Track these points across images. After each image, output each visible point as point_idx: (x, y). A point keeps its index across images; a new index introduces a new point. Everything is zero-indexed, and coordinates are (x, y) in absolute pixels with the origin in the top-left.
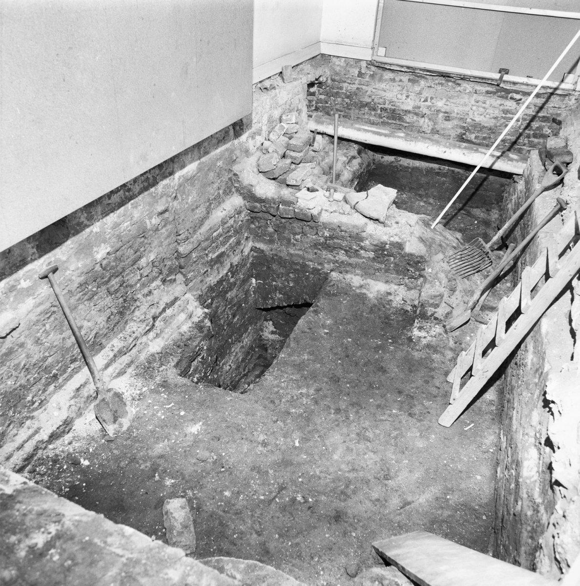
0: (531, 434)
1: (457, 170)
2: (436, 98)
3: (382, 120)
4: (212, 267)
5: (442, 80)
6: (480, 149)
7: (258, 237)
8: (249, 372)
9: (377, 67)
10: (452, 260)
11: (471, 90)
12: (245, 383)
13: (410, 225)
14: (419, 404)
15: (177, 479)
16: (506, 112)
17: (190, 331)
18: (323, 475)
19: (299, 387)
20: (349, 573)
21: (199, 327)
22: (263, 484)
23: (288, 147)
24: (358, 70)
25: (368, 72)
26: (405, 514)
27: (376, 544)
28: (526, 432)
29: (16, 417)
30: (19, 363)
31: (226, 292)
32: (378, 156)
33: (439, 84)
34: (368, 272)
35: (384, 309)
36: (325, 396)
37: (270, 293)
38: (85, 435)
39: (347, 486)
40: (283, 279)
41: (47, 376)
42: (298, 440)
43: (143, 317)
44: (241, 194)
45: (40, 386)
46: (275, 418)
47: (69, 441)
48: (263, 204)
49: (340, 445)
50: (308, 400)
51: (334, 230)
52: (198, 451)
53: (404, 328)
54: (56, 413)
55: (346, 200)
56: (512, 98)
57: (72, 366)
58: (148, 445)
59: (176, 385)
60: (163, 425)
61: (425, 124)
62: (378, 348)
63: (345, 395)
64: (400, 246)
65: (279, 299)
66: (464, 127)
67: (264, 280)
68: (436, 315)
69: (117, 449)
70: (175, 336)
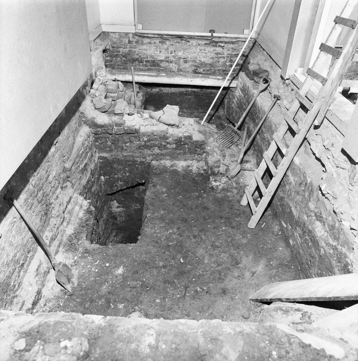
0: (312, 215)
1: (194, 90)
2: (177, 50)
3: (147, 68)
4: (83, 173)
5: (179, 40)
6: (209, 77)
7: (101, 149)
8: (109, 235)
9: (139, 36)
10: (218, 140)
11: (196, 44)
12: (109, 242)
13: (191, 125)
14: (234, 221)
15: (125, 303)
16: (217, 54)
17: (84, 216)
18: (204, 273)
19: (167, 230)
20: (245, 317)
21: (88, 212)
22: (175, 289)
23: (107, 91)
24: (128, 39)
25: (134, 40)
26: (256, 278)
27: (251, 297)
28: (309, 215)
29: (8, 298)
30: (4, 262)
31: (91, 188)
32: (149, 90)
33: (177, 42)
34: (173, 156)
35: (190, 175)
36: (183, 231)
37: (114, 183)
38: (52, 297)
39: (220, 275)
40: (122, 172)
41: (18, 266)
42: (182, 259)
43: (57, 214)
44: (87, 125)
45: (16, 274)
46: (163, 251)
47: (44, 304)
48: (103, 129)
49: (206, 254)
50: (176, 236)
51: (150, 136)
52: (129, 283)
53: (206, 183)
54: (30, 289)
55: (151, 117)
56: (219, 46)
57: (29, 256)
58: (96, 289)
59: (94, 250)
60: (99, 274)
61: (174, 67)
62: (198, 197)
63: (194, 227)
64: (190, 137)
65: (121, 185)
66: (195, 66)
67: (109, 175)
68: (220, 172)
69: (78, 298)
70: (78, 221)
